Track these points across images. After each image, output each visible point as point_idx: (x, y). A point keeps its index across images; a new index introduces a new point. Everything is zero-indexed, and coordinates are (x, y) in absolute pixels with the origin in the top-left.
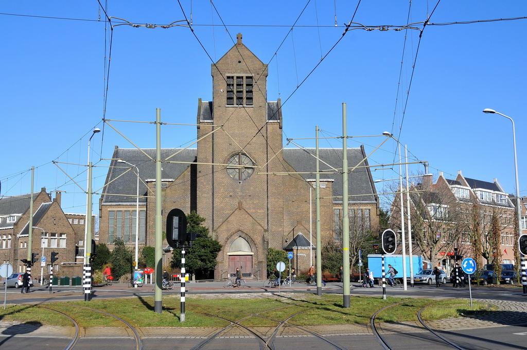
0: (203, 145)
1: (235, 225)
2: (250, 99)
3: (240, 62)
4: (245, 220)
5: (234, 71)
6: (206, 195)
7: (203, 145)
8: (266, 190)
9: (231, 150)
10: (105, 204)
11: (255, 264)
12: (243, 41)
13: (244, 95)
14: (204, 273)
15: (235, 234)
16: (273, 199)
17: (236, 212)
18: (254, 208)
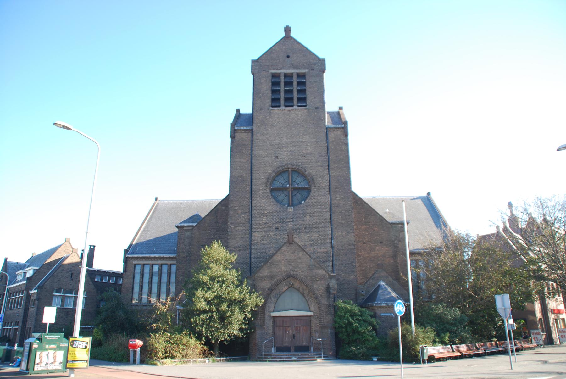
0: (238, 160)
1: (283, 268)
2: (302, 100)
3: (288, 57)
4: (299, 261)
5: (281, 67)
6: (240, 228)
7: (238, 160)
8: (329, 220)
9: (276, 164)
10: (130, 256)
11: (316, 331)
12: (293, 34)
13: (295, 95)
14: (532, 343)
15: (284, 283)
16: (340, 233)
17: (284, 248)
18: (312, 246)
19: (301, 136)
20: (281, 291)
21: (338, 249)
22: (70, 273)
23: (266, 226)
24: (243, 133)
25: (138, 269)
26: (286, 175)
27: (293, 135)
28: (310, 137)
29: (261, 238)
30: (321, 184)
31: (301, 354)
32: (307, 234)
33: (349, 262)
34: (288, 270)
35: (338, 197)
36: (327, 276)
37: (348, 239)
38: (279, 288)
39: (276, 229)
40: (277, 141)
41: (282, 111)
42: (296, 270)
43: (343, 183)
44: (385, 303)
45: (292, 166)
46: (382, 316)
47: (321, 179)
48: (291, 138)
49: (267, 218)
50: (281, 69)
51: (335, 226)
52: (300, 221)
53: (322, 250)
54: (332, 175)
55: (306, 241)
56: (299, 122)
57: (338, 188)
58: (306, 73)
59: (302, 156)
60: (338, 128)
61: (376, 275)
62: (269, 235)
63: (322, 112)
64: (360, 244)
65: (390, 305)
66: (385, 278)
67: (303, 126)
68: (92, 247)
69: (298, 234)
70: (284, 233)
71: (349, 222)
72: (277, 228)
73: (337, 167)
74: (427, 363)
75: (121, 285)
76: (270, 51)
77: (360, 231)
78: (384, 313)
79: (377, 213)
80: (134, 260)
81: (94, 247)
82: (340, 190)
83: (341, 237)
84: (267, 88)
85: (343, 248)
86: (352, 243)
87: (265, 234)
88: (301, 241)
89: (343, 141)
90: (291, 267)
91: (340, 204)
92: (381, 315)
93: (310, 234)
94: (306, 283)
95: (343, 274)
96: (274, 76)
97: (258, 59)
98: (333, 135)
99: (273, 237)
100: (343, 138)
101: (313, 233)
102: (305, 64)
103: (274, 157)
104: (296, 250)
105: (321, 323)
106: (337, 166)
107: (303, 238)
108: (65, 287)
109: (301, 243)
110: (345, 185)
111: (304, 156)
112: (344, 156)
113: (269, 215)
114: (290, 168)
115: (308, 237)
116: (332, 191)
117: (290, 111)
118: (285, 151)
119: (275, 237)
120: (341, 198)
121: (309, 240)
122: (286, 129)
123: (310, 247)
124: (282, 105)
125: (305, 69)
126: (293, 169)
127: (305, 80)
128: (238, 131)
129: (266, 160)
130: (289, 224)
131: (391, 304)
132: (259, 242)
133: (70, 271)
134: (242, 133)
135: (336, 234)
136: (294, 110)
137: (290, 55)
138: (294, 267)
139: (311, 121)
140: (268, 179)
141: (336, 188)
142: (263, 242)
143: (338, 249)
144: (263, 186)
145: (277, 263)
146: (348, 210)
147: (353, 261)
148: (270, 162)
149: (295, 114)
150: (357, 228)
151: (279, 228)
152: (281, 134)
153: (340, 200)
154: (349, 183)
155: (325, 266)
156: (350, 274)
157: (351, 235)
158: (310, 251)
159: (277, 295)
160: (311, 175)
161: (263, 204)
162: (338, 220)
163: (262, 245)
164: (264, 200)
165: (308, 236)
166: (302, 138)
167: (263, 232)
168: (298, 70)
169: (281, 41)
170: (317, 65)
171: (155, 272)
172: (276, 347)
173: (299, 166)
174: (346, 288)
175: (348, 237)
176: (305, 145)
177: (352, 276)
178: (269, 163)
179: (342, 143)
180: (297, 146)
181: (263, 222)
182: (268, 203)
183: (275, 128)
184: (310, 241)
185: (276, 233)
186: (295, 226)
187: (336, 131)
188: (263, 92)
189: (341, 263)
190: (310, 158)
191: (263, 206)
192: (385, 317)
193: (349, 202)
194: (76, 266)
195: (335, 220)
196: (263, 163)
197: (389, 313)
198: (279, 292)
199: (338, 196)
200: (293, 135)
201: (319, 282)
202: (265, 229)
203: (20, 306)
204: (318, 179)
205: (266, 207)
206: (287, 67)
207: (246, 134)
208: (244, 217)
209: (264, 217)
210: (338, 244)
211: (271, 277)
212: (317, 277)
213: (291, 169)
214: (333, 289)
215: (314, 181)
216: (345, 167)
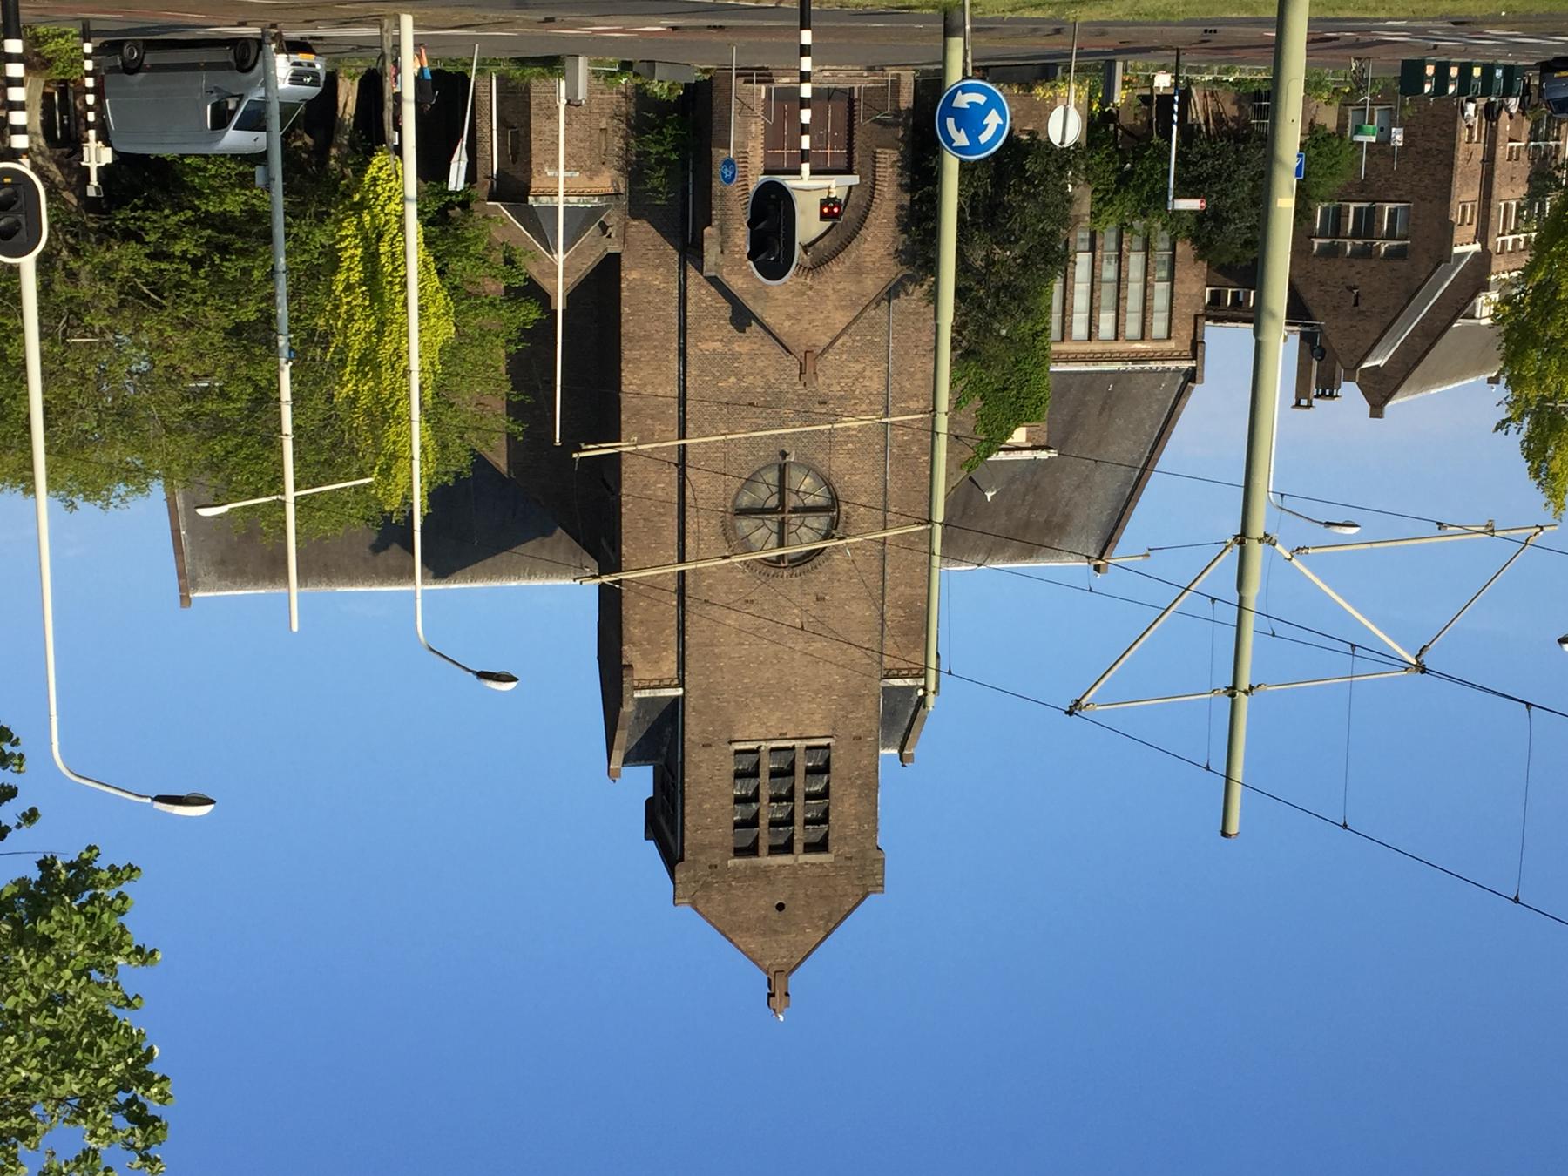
1: (830, 292)
3: (780, 907)
4: (791, 310)
19: (753, 660)
21: (667, 349)
22: (1362, 307)
25: (1159, 327)
28: (730, 658)
29: (864, 378)
32: (747, 388)
34: (819, 287)
39: (825, 403)
42: (799, 287)
45: (780, 574)
48: (780, 655)
53: (710, 346)
56: (758, 700)
58: (732, 855)
59: (752, 601)
60: (649, 687)
67: (747, 690)
68: (1304, 402)
69: (770, 387)
75: (1208, 286)
80: (1173, 352)
81: (1298, 405)
82: (653, 508)
84: (844, 807)
88: (762, 371)
90: (810, 293)
91: (655, 472)
92: (578, 174)
96: (821, 846)
98: (665, 669)
99: (834, 382)
102: (733, 883)
108: (1373, 263)
109: (762, 364)
110: (641, 523)
118: (797, 616)
119: (828, 381)
122: (793, 680)
124: (803, 751)
132: (868, 368)
133: (1362, 312)
135: (669, 389)
137: (775, 914)
138: (804, 294)
139: (725, 704)
142: (859, 367)
143: (667, 349)
144: (855, 518)
145: (844, 303)
148: (836, 584)
149: (768, 727)
153: (656, 482)
155: (704, 305)
156: (638, 283)
161: (856, 469)
163: (861, 359)
164: (854, 478)
166: (750, 653)
167: (857, 392)
171: (1107, 309)
178: (839, 581)
182: (844, 472)
183: (823, 683)
184: (741, 371)
188: (854, 790)
190: (732, 597)
191: (856, 464)
194: (1346, 330)
196: (855, 580)
199: (660, 493)
202: (853, 402)
203: (1464, 208)
207: (897, 666)
209: (854, 432)
211: (858, 271)
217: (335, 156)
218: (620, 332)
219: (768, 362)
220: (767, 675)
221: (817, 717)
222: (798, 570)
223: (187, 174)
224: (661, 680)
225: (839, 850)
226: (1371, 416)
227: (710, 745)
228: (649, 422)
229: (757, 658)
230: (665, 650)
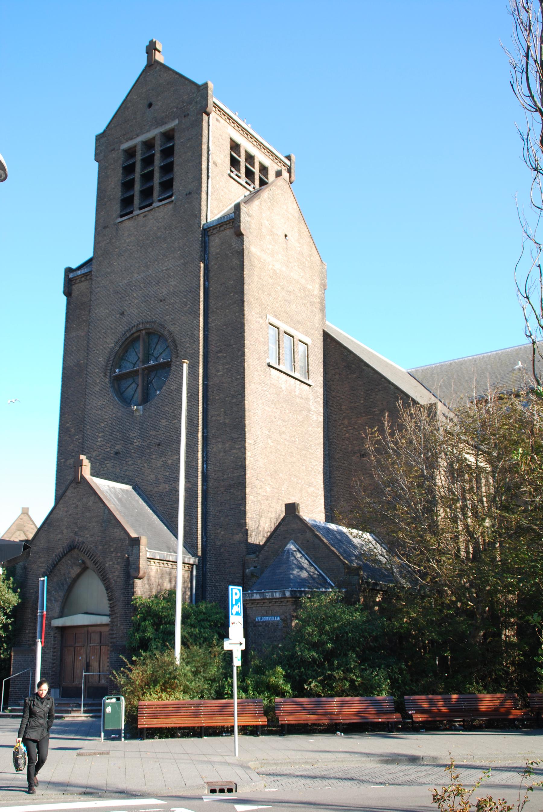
1: (65, 531)
16: (220, 446)
20: (69, 578)
21: (215, 480)
23: (103, 451)
24: (84, 281)
26: (140, 347)
27: (149, 263)
30: (188, 350)
31: (59, 704)
32: (161, 457)
33: (234, 506)
35: (221, 369)
36: (127, 542)
37: (234, 457)
38: (62, 572)
40: (125, 281)
41: (135, 219)
43: (229, 338)
44: (259, 593)
46: (259, 622)
47: (187, 339)
49: (103, 437)
50: (138, 135)
51: (213, 431)
52: (151, 433)
54: (213, 324)
55: (159, 470)
56: (159, 234)
57: (220, 351)
59: (161, 301)
61: (282, 529)
62: (106, 469)
63: (197, 198)
64: (353, 458)
65: (268, 597)
66: (299, 535)
69: (147, 460)
70: (127, 460)
71: (237, 420)
72: (117, 453)
73: (221, 306)
74: (123, 739)
76: (124, 106)
77: (354, 428)
78: (263, 615)
79: (389, 382)
82: (225, 355)
83: (222, 454)
85: (225, 476)
86: (240, 463)
87: (100, 467)
88: (152, 471)
89: (235, 247)
90: (76, 530)
91: (223, 383)
93: (165, 456)
94: (95, 557)
95: (222, 533)
97: (105, 131)
98: (217, 240)
100: (234, 241)
101: (170, 453)
102: (175, 109)
103: (118, 316)
104: (84, 495)
105: (112, 638)
106: (220, 304)
107: (154, 466)
111: (164, 300)
112: (234, 281)
113: (107, 429)
114: (142, 330)
115: (162, 463)
116: (210, 360)
117: (146, 216)
120: (225, 370)
121: (163, 468)
123: (165, 482)
125: (173, 119)
126: (147, 331)
127: (171, 144)
128: (76, 280)
129: (107, 323)
130: (135, 441)
131: (270, 594)
134: (81, 281)
136: (152, 212)
140: (108, 360)
141: (217, 353)
143: (215, 480)
146: (237, 393)
147: (240, 502)
150: (348, 423)
151: (120, 451)
152: (132, 266)
153: (222, 376)
154: (240, 335)
157: (240, 446)
158: (165, 491)
159: (63, 584)
160: (172, 335)
162: (219, 418)
165: (163, 461)
168: (163, 126)
169: (141, 77)
170: (193, 103)
172: (63, 687)
173: (155, 322)
174: (226, 561)
175: (235, 451)
176: (167, 276)
177: (237, 536)
178: (112, 329)
179: (232, 253)
180: (154, 283)
181: (98, 444)
183: (122, 257)
185: (115, 462)
186: (144, 444)
187: (223, 231)
189: (220, 508)
191: (100, 413)
192: (264, 624)
193: (239, 377)
195: (213, 418)
197: (272, 615)
198: (65, 580)
199: (220, 368)
200: (149, 263)
201: (113, 555)
202: (100, 457)
204: (183, 340)
205: (103, 414)
206: (147, 128)
208: (78, 439)
209: (100, 435)
210: (217, 469)
212: (111, 544)
213: (144, 332)
214: (134, 568)
215: (176, 346)
216: (235, 303)
217: (327, 643)
218: (245, 492)
219: (149, 478)
220: (152, 253)
221: (126, 234)
222: (134, 330)
223: (465, 620)
224: (219, 231)
225: (118, 153)
226: (28, 508)
227: (187, 195)
228: (227, 421)
229: (159, 262)
230: (217, 254)
